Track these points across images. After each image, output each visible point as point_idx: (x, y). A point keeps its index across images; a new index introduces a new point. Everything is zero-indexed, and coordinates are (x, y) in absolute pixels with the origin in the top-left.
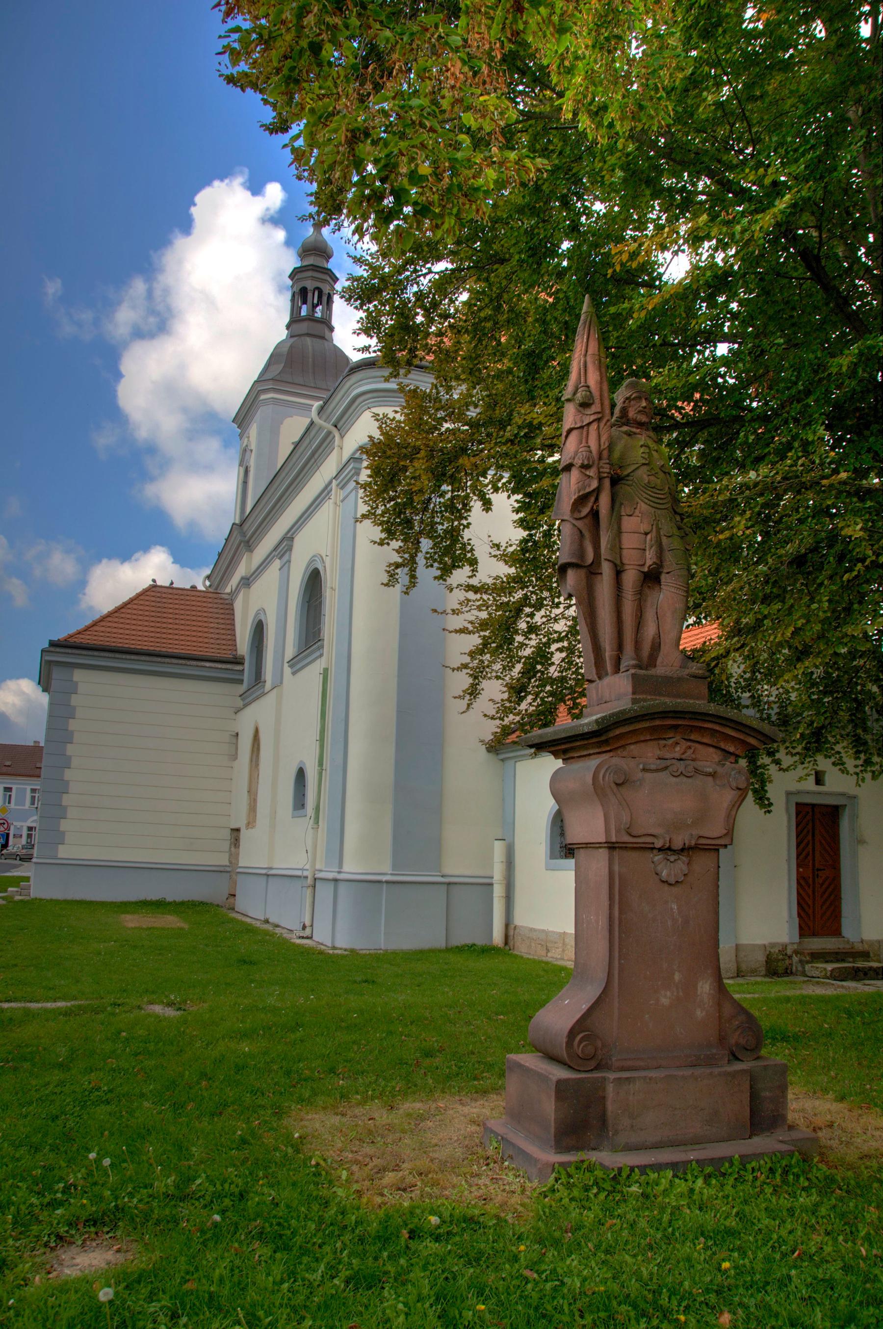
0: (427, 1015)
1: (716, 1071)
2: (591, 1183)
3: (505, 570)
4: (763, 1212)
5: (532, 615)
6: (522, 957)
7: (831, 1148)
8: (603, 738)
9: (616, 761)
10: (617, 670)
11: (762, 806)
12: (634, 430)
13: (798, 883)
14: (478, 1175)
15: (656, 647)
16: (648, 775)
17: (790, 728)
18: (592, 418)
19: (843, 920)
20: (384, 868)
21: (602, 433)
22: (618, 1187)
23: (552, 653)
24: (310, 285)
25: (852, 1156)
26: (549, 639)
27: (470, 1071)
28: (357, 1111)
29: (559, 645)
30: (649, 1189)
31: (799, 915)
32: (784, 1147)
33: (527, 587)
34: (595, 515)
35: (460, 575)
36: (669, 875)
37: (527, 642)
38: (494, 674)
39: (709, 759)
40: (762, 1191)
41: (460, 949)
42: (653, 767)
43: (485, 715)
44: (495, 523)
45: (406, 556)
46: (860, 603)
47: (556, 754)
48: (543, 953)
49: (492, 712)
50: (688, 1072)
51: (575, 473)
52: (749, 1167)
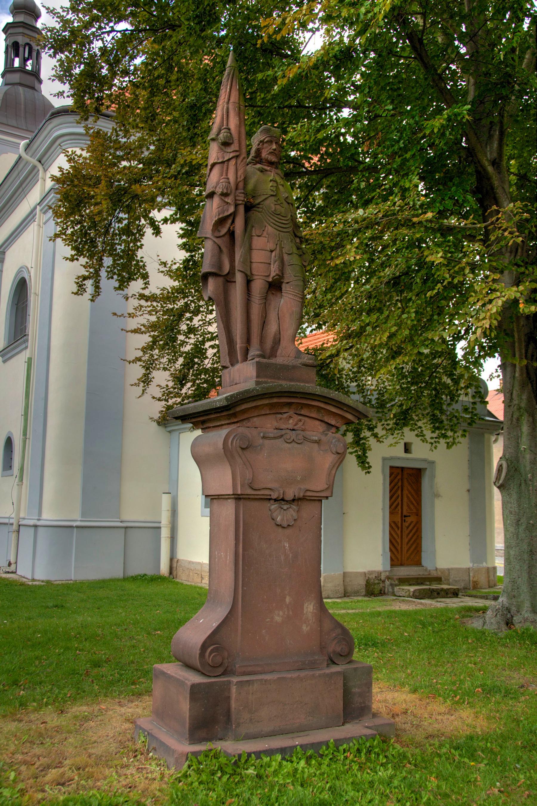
0: (100, 632)
1: (317, 673)
2: (216, 769)
3: (171, 283)
4: (349, 786)
5: (191, 319)
6: (182, 584)
7: (405, 730)
8: (231, 412)
9: (241, 430)
10: (245, 359)
11: (364, 468)
12: (266, 168)
13: (390, 525)
14: (127, 766)
15: (277, 341)
16: (267, 442)
17: (386, 410)
18: (232, 155)
19: (423, 554)
20: (75, 517)
21: (239, 168)
22: (238, 770)
23: (206, 349)
24: (21, 40)
25: (420, 736)
26: (204, 338)
27: (129, 678)
28: (32, 717)
29: (212, 343)
30: (263, 770)
31: (391, 550)
32: (369, 732)
33: (188, 297)
34: (231, 234)
35: (136, 286)
36: (282, 520)
37: (187, 340)
38: (162, 366)
39: (315, 429)
40: (351, 767)
41: (134, 579)
42: (271, 435)
43: (154, 398)
44: (164, 245)
45: (91, 270)
46: (439, 314)
47: (196, 425)
48: (199, 580)
49: (159, 395)
50: (295, 675)
51: (216, 200)
52: (341, 748)
